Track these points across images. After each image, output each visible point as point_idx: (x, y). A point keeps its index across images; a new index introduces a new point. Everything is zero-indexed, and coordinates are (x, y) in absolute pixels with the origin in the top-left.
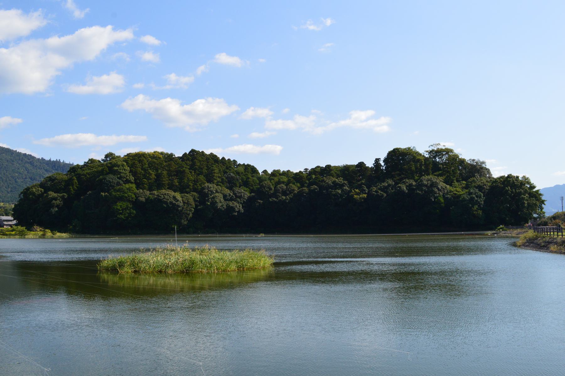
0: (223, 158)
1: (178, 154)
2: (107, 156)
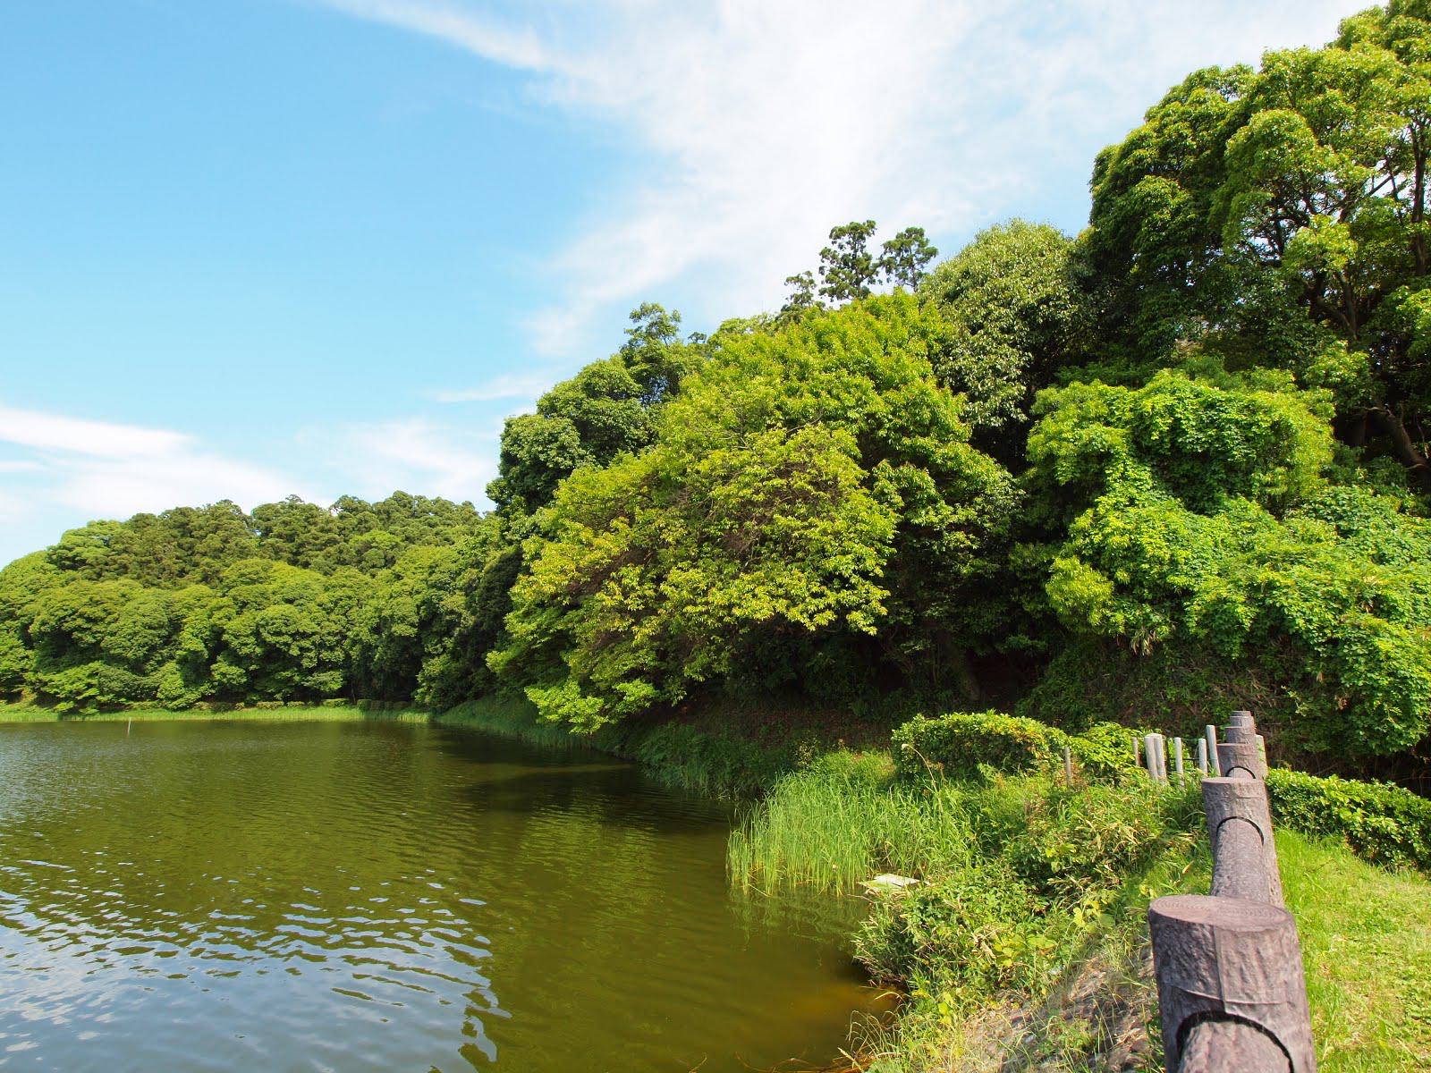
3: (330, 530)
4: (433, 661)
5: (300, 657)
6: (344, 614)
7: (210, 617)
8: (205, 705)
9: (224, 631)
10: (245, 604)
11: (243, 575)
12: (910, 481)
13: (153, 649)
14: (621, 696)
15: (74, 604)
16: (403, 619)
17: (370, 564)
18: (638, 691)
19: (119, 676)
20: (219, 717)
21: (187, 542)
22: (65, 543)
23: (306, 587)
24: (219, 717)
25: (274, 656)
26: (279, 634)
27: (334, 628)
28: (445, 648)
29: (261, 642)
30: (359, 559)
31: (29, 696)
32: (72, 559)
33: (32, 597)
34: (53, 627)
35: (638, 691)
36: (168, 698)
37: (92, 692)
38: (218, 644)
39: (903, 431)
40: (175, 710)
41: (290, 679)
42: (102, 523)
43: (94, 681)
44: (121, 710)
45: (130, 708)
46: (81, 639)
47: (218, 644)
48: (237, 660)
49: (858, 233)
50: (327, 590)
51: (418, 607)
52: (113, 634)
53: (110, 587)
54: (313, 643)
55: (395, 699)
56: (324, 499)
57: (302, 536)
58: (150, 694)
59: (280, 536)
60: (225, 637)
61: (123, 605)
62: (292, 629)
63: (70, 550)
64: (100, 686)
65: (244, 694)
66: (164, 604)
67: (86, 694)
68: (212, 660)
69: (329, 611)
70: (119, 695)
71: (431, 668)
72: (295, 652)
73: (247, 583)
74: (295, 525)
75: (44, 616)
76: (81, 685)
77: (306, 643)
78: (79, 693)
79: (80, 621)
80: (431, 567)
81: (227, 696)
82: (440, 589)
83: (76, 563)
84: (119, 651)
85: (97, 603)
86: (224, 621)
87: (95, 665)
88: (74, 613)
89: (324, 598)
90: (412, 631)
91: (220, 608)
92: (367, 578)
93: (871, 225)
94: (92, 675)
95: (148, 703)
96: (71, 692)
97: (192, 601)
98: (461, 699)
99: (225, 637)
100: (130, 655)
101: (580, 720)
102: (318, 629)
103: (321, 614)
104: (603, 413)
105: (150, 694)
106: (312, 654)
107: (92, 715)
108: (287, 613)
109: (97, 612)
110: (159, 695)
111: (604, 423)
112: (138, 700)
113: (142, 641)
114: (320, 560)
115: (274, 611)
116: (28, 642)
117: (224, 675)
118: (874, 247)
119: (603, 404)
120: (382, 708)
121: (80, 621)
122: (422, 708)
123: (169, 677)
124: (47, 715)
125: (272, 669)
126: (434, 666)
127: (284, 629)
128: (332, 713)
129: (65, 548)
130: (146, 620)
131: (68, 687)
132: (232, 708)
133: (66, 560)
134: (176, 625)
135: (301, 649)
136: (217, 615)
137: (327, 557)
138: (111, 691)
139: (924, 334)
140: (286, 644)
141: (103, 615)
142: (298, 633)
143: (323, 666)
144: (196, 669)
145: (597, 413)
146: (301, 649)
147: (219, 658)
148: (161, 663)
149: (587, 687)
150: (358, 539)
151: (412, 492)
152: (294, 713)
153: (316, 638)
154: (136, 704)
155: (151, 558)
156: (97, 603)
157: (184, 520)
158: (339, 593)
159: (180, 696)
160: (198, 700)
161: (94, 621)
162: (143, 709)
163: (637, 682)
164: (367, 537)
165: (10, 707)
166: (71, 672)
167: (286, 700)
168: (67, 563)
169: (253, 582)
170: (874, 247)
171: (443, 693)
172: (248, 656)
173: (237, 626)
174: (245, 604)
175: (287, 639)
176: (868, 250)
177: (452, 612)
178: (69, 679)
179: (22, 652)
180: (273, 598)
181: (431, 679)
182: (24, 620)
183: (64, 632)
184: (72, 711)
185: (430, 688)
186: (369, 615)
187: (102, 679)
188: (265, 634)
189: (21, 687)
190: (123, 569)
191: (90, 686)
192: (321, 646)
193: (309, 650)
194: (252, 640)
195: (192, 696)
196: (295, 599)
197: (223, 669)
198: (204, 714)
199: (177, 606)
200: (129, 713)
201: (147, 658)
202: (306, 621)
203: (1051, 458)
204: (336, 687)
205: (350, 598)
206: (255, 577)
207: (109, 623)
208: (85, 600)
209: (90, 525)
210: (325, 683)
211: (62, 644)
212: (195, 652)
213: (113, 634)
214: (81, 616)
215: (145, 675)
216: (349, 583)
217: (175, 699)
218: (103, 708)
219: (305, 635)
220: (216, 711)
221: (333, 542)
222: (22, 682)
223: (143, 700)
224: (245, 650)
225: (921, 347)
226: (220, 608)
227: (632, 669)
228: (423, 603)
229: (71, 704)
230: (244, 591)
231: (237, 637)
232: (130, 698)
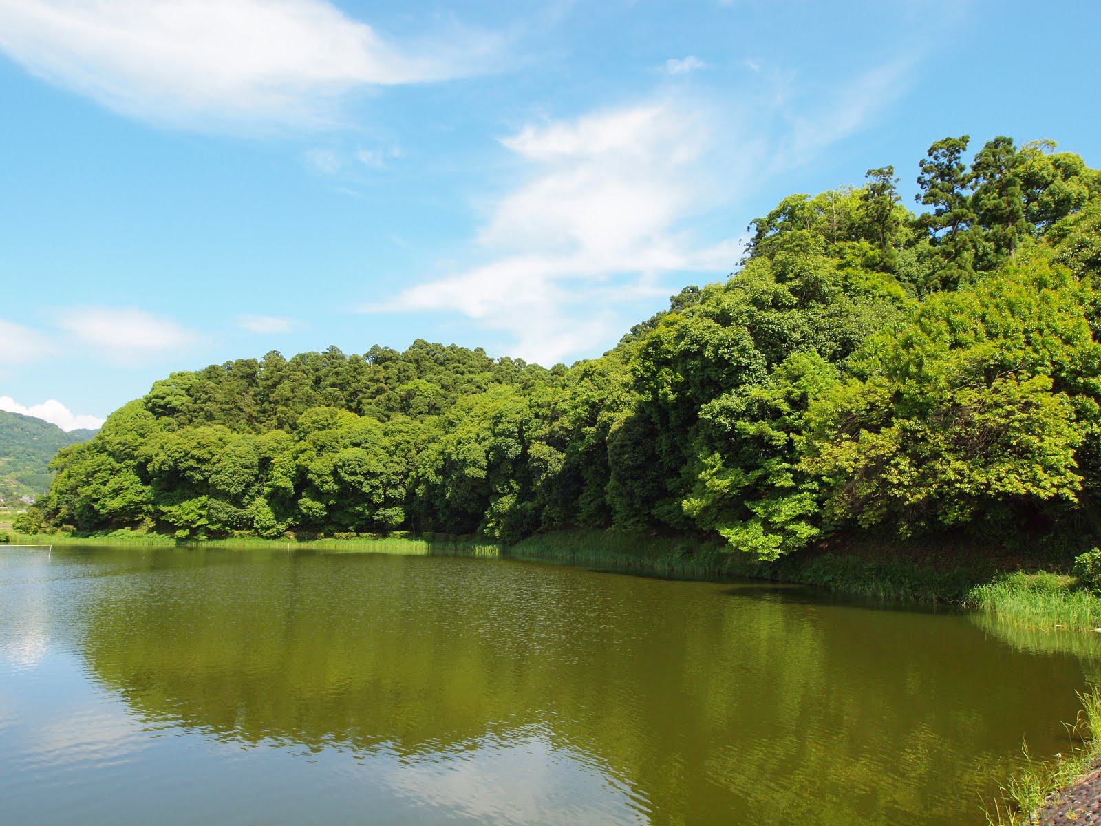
3: (378, 381)
4: (501, 499)
5: (371, 493)
6: (404, 457)
7: (295, 458)
8: (291, 534)
9: (307, 471)
10: (321, 448)
11: (315, 422)
12: (1084, 406)
13: (248, 485)
14: (794, 533)
15: (187, 448)
16: (475, 463)
17: (417, 411)
18: (805, 531)
19: (224, 509)
20: (305, 545)
21: (255, 390)
22: (156, 392)
23: (369, 432)
24: (305, 545)
26: (354, 473)
27: (398, 469)
28: (511, 488)
29: (339, 480)
30: (405, 405)
31: (149, 522)
32: (164, 407)
33: (142, 440)
34: (170, 466)
35: (805, 531)
36: (262, 528)
37: (203, 521)
38: (303, 481)
39: (1079, 374)
40: (267, 538)
41: (362, 513)
42: (182, 375)
43: (204, 513)
44: (225, 538)
45: (232, 536)
46: (192, 476)
47: (303, 481)
48: (318, 495)
49: (954, 148)
50: (386, 434)
51: (487, 453)
52: (218, 473)
53: (208, 432)
54: (381, 482)
55: (459, 533)
56: (355, 347)
57: (354, 385)
58: (246, 524)
59: (333, 385)
60: (310, 476)
61: (222, 448)
62: (364, 469)
63: (163, 398)
64: (209, 517)
65: (322, 525)
66: (253, 447)
67: (199, 523)
68: (298, 496)
69: (391, 454)
70: (225, 524)
71: (501, 506)
72: (366, 489)
73: (320, 429)
74: (345, 375)
75: (163, 457)
76: (193, 516)
77: (375, 482)
78: (193, 522)
79: (192, 462)
80: (496, 417)
81: (308, 527)
82: (508, 437)
83: (171, 411)
84: (223, 487)
85: (204, 447)
86: (308, 462)
87: (204, 499)
88: (186, 455)
89: (386, 442)
90: (482, 474)
91: (303, 451)
92: (417, 423)
93: (965, 140)
94: (203, 507)
95: (246, 532)
96: (187, 521)
97: (275, 445)
98: (526, 534)
99: (310, 476)
100: (232, 490)
101: (766, 551)
102: (384, 469)
103: (385, 457)
104: (773, 323)
105: (246, 524)
106: (381, 491)
107: (205, 543)
108: (360, 455)
109: (204, 454)
110: (255, 525)
111: (773, 331)
112: (237, 529)
113: (240, 479)
114: (373, 407)
115: (350, 453)
116: (145, 478)
117: (309, 508)
118: (967, 159)
119: (771, 315)
120: (447, 540)
121: (192, 462)
122: (490, 540)
123: (260, 509)
124: (164, 542)
125: (348, 506)
126: (505, 503)
127: (358, 470)
128: (398, 545)
129: (156, 397)
130: (243, 461)
131: (185, 517)
132: (314, 538)
133: (159, 407)
134: (265, 463)
135: (372, 486)
136: (302, 457)
137: (378, 404)
138: (219, 521)
139: (1081, 301)
140: (360, 483)
141: (209, 456)
142: (369, 473)
143: (389, 502)
144: (282, 503)
145: (768, 322)
146: (372, 486)
147: (303, 494)
148: (253, 497)
149: (769, 527)
150: (402, 389)
151: (431, 340)
152: (364, 544)
153: (383, 477)
154: (236, 533)
155: (232, 406)
156: (204, 447)
157: (250, 371)
158: (399, 438)
159: (273, 526)
160: (286, 530)
162: (242, 536)
163: (803, 523)
164: (410, 386)
165: (134, 533)
166: (185, 504)
167: (359, 531)
168: (160, 410)
169: (324, 427)
170: (967, 159)
171: (511, 528)
172: (328, 492)
173: (319, 465)
174: (321, 448)
175: (360, 478)
176: (962, 162)
177: (539, 459)
178: (186, 510)
179: (141, 487)
180: (342, 442)
181: (499, 515)
182: (141, 459)
183: (179, 471)
184: (187, 538)
185: (498, 523)
186: (433, 458)
187: (211, 511)
188: (343, 474)
189: (140, 516)
190: (210, 417)
191: (201, 516)
192: (389, 484)
193: (378, 488)
194: (330, 478)
195: (282, 527)
196: (359, 443)
197: (308, 504)
198: (290, 544)
199: (264, 449)
200: (232, 540)
201: (244, 493)
202: (374, 462)
203: (1037, 759)
204: (401, 520)
205: (408, 442)
206: (326, 423)
207: (214, 463)
208: (194, 444)
209: (173, 376)
210: (391, 517)
211: (175, 481)
212: (285, 489)
213: (218, 473)
214: (193, 457)
215: (242, 507)
216: (406, 429)
217: (268, 528)
218: (212, 535)
219: (374, 475)
220: (300, 539)
221: (379, 391)
222: (142, 511)
223: (242, 529)
224: (326, 487)
225: (1080, 310)
226: (303, 451)
227: (800, 514)
228: (492, 449)
229: (187, 532)
230: (323, 436)
231: (319, 476)
232: (233, 527)
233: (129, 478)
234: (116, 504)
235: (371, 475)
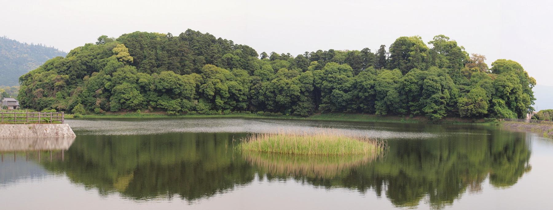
0: (220, 38)
1: (176, 34)
2: (100, 39)
25: (233, 96)
146: (240, 94)
161: (180, 85)
173: (224, 87)
196: (222, 78)
229: (174, 112)
233: (136, 92)
234: (136, 102)
235: (240, 90)
